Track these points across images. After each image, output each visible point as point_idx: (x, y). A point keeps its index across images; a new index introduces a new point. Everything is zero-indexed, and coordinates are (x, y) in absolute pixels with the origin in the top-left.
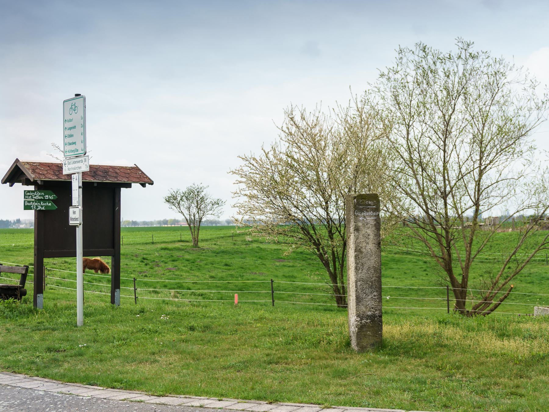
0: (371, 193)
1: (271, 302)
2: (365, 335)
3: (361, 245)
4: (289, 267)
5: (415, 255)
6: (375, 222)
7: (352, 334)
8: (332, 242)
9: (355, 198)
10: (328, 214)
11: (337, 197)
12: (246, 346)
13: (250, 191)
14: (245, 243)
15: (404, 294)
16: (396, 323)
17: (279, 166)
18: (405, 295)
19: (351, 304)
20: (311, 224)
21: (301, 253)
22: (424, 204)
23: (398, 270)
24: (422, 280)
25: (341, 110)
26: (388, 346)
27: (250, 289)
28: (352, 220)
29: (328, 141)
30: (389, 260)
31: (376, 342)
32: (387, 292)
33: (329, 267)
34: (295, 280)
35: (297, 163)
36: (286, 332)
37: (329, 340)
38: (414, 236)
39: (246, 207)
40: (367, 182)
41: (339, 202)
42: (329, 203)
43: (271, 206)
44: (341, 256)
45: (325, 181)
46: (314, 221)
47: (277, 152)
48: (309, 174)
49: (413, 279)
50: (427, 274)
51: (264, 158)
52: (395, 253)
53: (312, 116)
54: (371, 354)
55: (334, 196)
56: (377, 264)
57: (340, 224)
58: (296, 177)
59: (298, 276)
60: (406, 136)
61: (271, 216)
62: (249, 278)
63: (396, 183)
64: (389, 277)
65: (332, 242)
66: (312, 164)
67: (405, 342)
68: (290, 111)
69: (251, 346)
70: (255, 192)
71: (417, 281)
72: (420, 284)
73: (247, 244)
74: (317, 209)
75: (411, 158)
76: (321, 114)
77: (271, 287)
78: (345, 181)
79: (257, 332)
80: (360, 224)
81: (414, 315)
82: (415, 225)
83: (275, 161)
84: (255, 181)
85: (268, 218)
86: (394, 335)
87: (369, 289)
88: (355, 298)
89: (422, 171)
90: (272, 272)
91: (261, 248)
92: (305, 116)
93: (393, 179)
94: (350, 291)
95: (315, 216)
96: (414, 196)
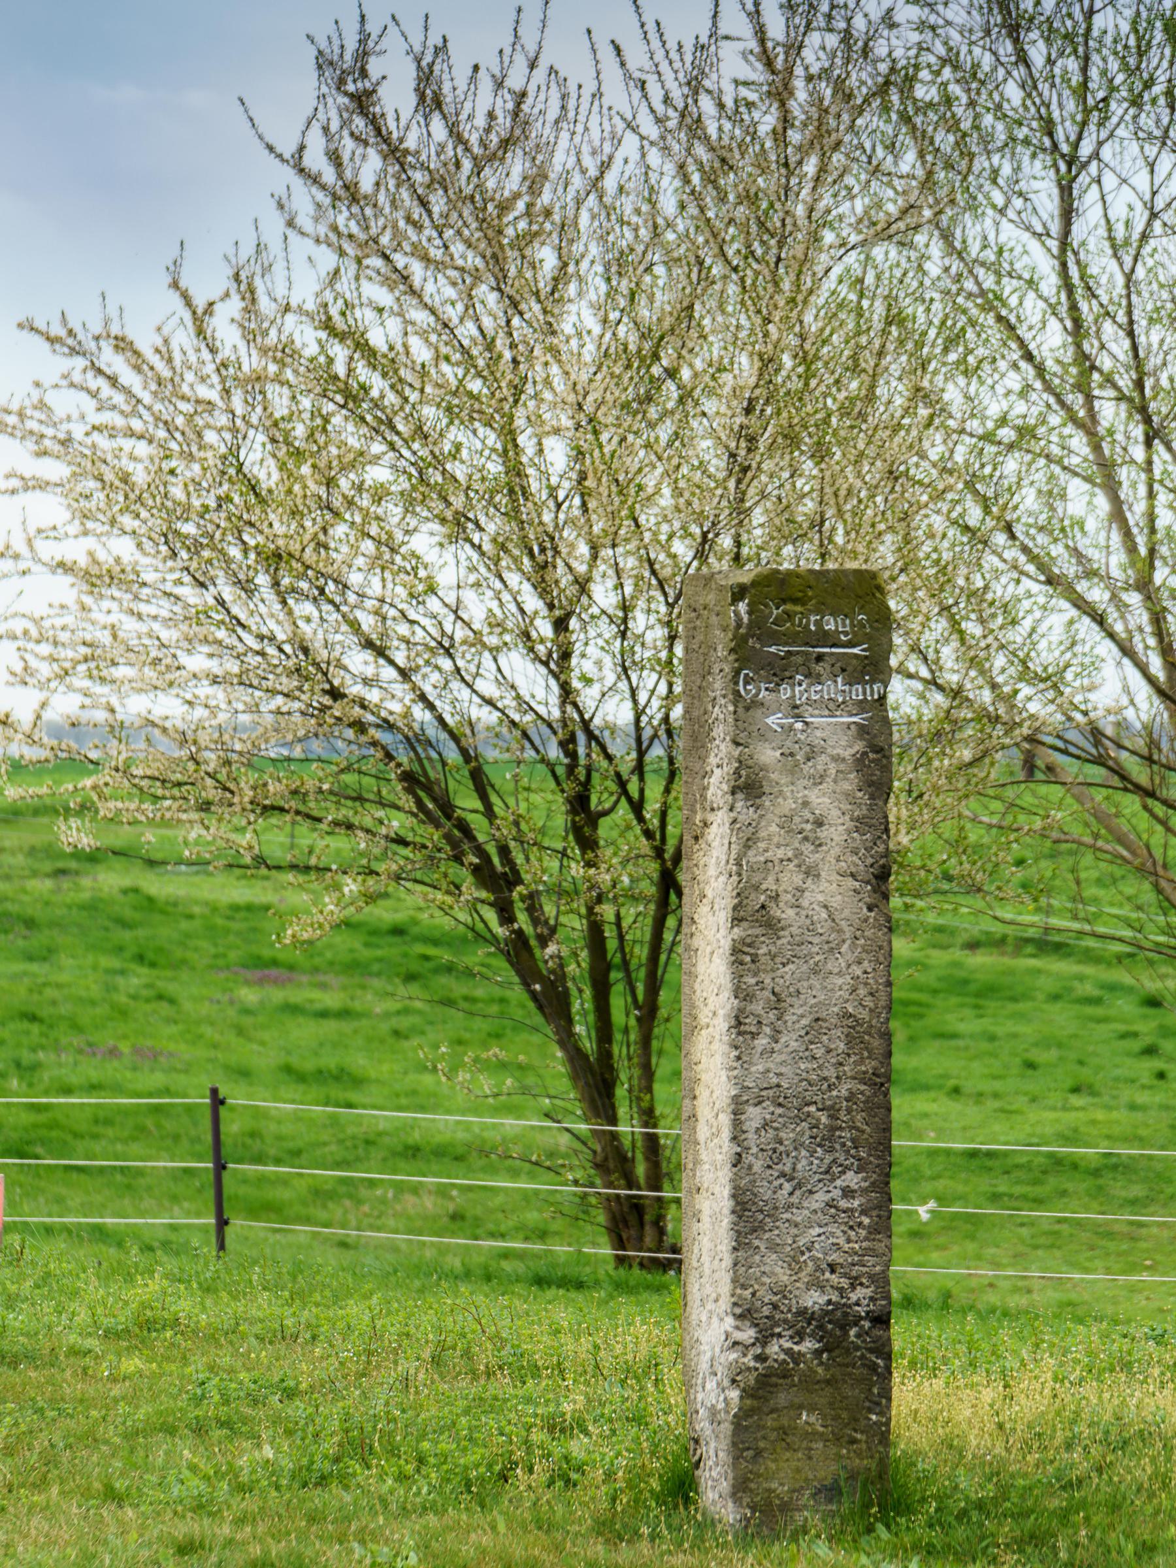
0: (831, 565)
1: (203, 1229)
2: (784, 1432)
3: (769, 884)
4: (324, 1014)
5: (1090, 957)
6: (859, 746)
7: (703, 1426)
8: (589, 864)
9: (739, 592)
10: (567, 693)
11: (628, 590)
12: (55, 1490)
13: (90, 542)
14: (48, 866)
15: (1018, 1190)
16: (972, 1364)
17: (272, 390)
18: (1024, 1197)
19: (705, 1242)
20: (464, 752)
21: (398, 931)
22: (1152, 642)
23: (985, 1046)
24: (1133, 1107)
25: (659, 55)
26: (923, 1500)
27: (81, 1146)
28: (719, 731)
29: (577, 248)
30: (935, 985)
31: (852, 1476)
32: (916, 1178)
33: (570, 1021)
34: (353, 1096)
35: (384, 375)
36: (298, 1409)
37: (566, 1458)
38: (1088, 839)
39: (64, 637)
40: (809, 505)
41: (639, 622)
42: (573, 623)
43: (221, 634)
44: (640, 953)
45: (552, 491)
46: (481, 736)
47: (265, 305)
48: (458, 447)
49: (1076, 1100)
50: (1161, 1075)
51: (183, 339)
52: (973, 946)
53: (485, 84)
54: (822, 1549)
55: (611, 583)
56: (869, 1002)
57: (641, 754)
58: (376, 460)
59: (373, 1074)
60: (1055, 228)
61: (219, 695)
62: (74, 1080)
63: (987, 510)
64: (927, 1088)
65: (589, 864)
66: (475, 386)
67: (1025, 1476)
68: (348, 56)
69: (87, 1493)
70: (123, 548)
71: (1100, 1115)
72: (1116, 1130)
73: (62, 872)
74: (502, 661)
75: (1086, 363)
76: (540, 74)
77: (209, 1138)
78: (677, 492)
79: (122, 1408)
80: (768, 755)
81: (1080, 1321)
82: (1096, 772)
83: (251, 362)
84: (125, 478)
85: (200, 712)
86: (963, 1437)
87: (812, 1153)
88: (727, 1204)
89: (1148, 443)
90: (215, 1046)
91: (150, 900)
92: (446, 88)
93: (970, 485)
94: (697, 1162)
95: (490, 702)
96: (1097, 595)
